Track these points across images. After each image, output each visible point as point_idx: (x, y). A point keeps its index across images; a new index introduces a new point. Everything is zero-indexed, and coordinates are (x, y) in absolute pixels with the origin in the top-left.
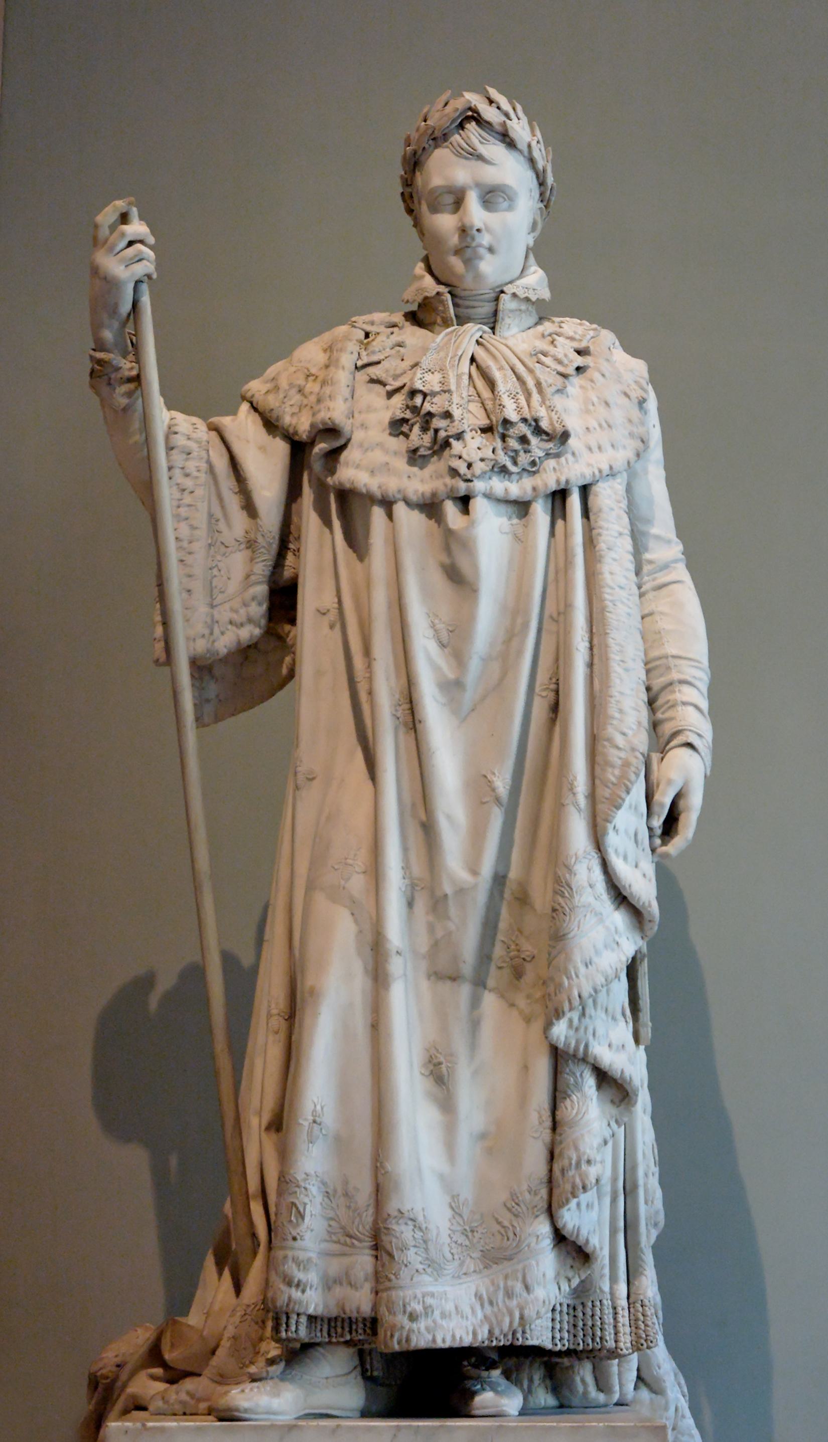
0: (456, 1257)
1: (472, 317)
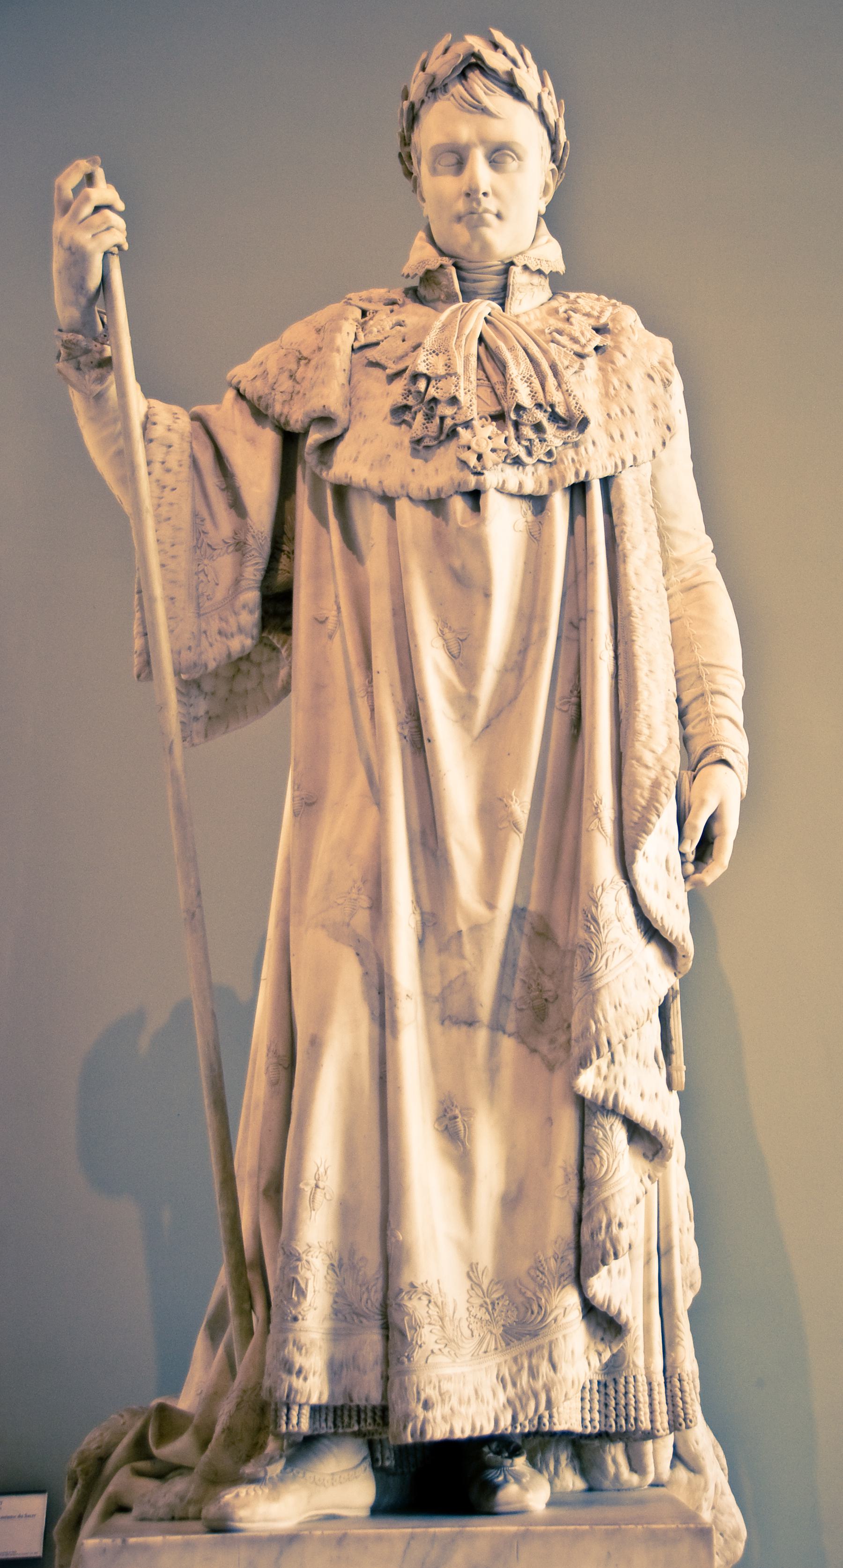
0: (476, 1333)
1: (480, 291)
